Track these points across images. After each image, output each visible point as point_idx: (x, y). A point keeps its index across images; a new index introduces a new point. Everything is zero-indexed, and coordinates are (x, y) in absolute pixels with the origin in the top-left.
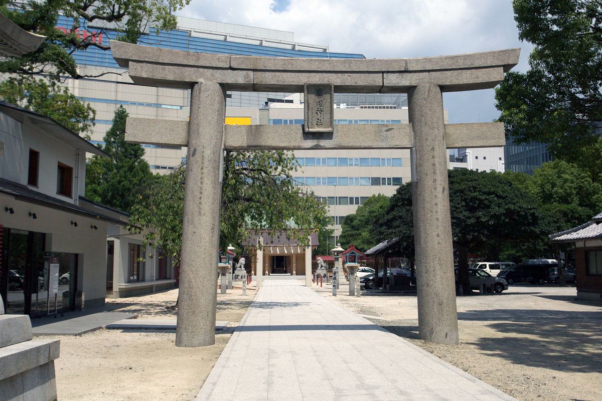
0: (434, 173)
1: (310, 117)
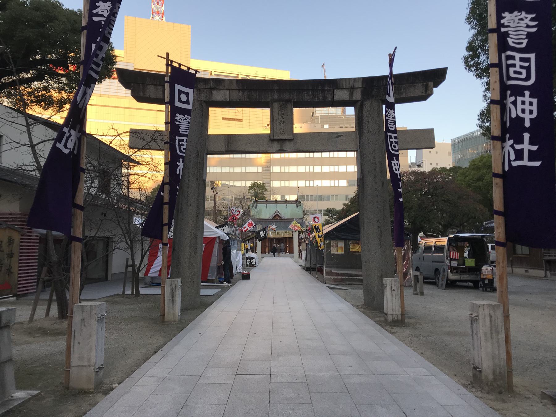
0: (375, 170)
1: (275, 127)
